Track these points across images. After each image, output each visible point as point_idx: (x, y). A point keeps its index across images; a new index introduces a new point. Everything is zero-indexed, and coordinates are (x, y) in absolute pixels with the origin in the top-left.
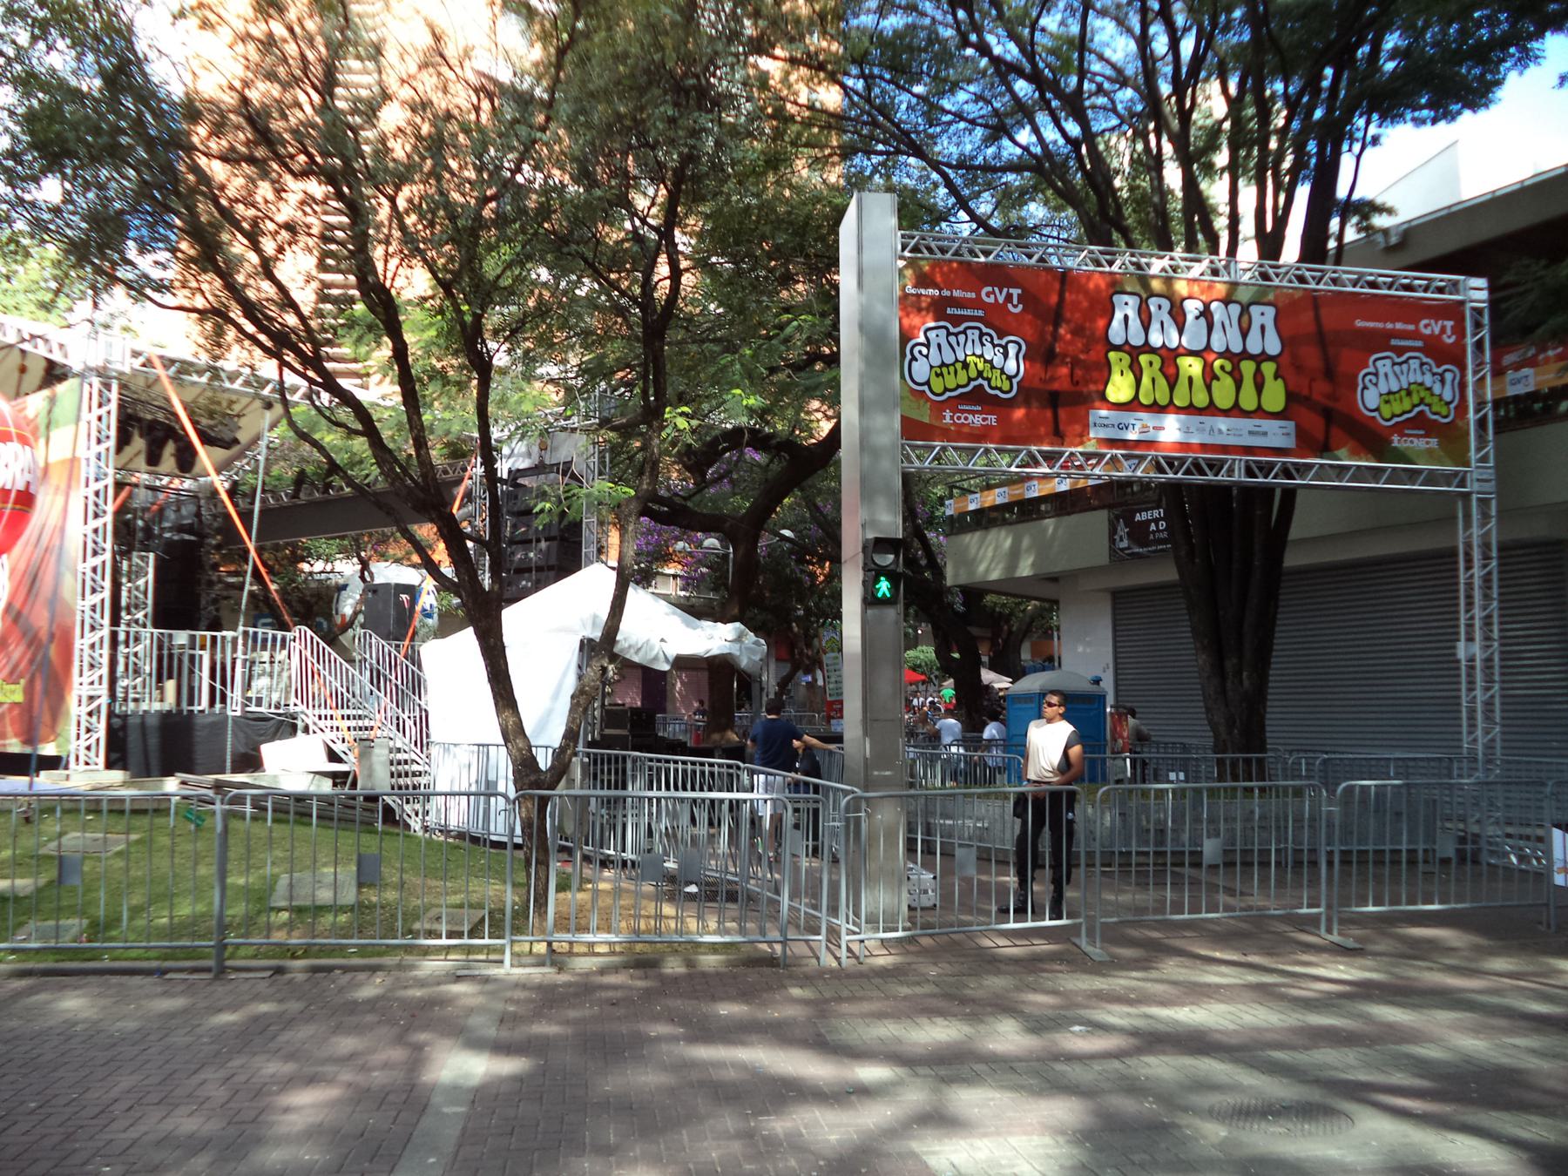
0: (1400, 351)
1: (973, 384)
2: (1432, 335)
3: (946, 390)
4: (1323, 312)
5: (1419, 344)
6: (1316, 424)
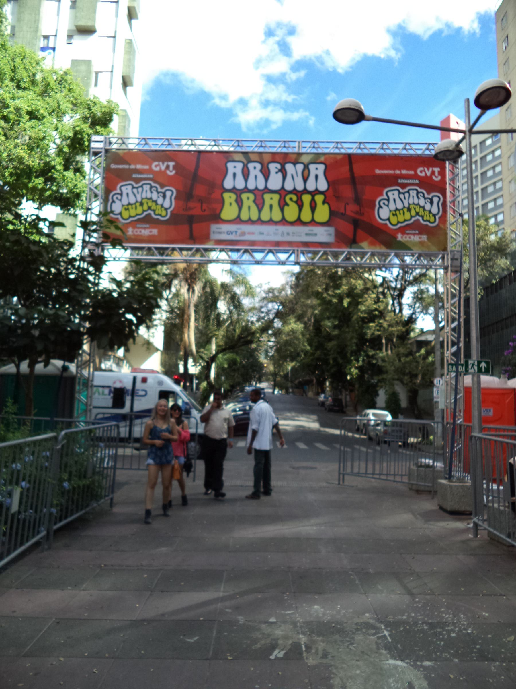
0: (403, 186)
1: (145, 213)
2: (160, 171)
3: (399, 222)
4: (355, 166)
5: (417, 181)
6: (348, 229)
